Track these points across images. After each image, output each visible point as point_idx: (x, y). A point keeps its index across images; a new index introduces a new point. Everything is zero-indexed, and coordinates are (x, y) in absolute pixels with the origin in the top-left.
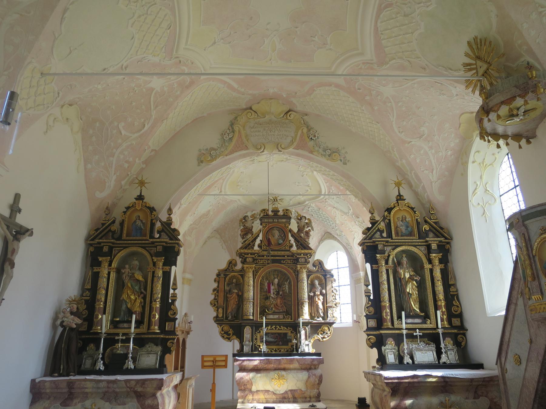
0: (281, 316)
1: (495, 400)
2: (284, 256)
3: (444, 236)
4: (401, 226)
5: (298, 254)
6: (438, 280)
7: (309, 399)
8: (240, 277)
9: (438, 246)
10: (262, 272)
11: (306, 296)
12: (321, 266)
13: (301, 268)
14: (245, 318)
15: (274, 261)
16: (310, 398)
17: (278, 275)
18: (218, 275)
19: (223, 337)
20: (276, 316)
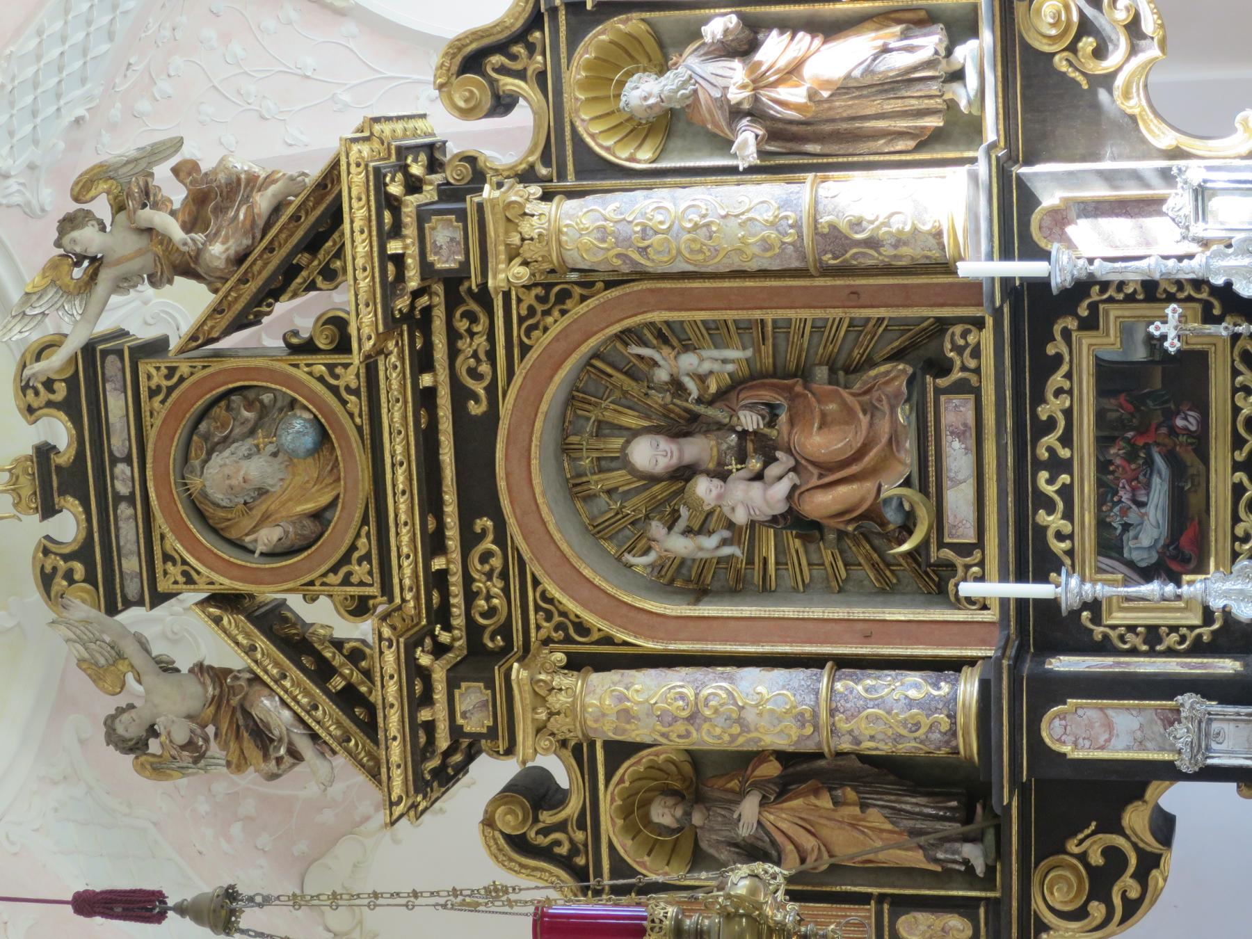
0: (956, 411)
2: (427, 398)
5: (391, 288)
8: (627, 769)
10: (582, 578)
12: (502, 47)
14: (969, 745)
15: (480, 495)
17: (603, 429)
19: (1132, 908)
20: (957, 458)
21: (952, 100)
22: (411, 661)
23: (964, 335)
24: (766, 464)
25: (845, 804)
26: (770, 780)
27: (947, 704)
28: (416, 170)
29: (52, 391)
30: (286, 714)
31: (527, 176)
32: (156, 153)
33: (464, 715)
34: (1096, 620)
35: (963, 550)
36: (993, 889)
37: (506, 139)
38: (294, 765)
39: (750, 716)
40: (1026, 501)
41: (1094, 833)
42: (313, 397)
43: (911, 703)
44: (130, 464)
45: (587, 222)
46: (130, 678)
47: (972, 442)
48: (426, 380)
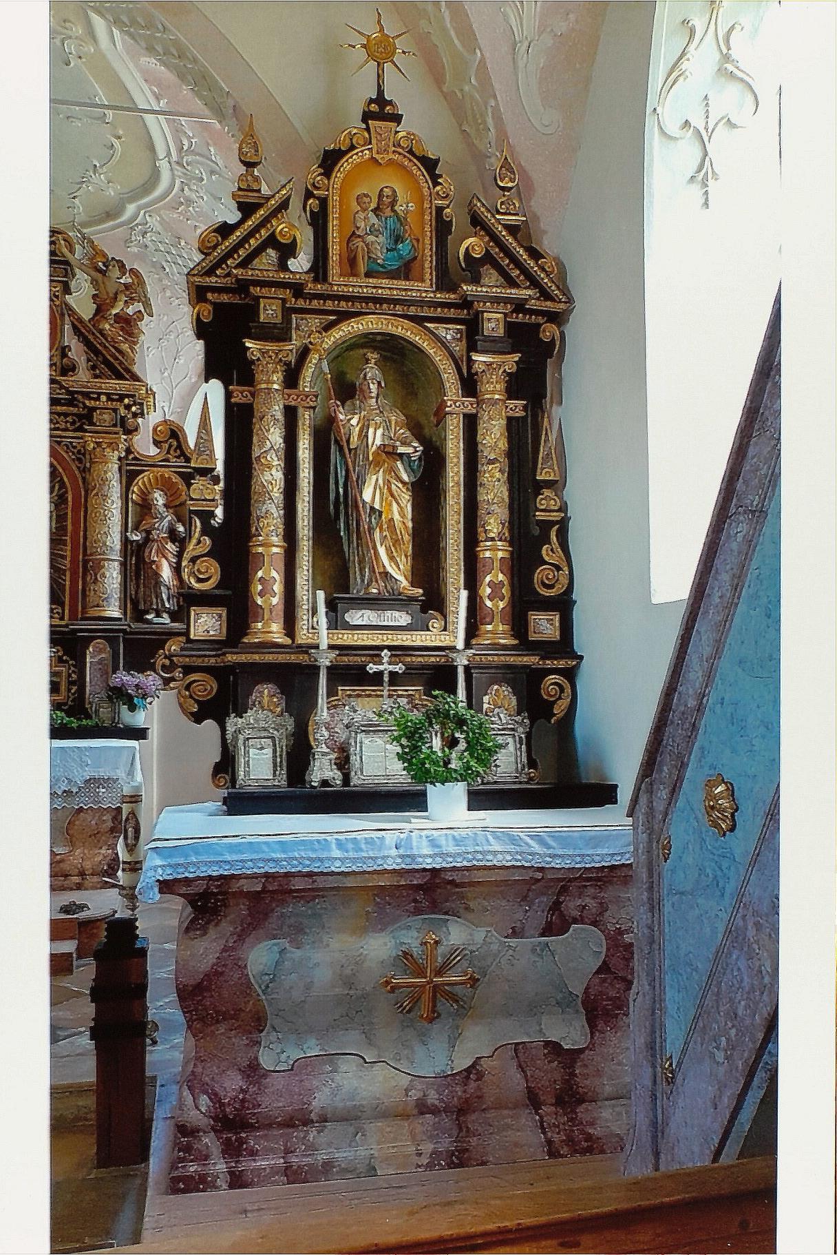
1: (627, 938)
3: (534, 283)
4: (373, 231)
5: (87, 395)
6: (491, 462)
7: (76, 879)
9: (510, 327)
11: (114, 540)
12: (179, 447)
16: (82, 874)
28: (134, 409)
31: (129, 451)
32: (147, 305)
37: (145, 445)
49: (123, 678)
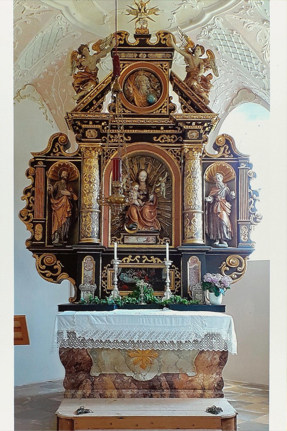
0: (152, 240)
2: (158, 128)
5: (185, 123)
7: (200, 392)
11: (199, 202)
12: (230, 148)
13: (190, 149)
15: (136, 138)
16: (203, 389)
18: (33, 164)
19: (44, 275)
20: (142, 239)
21: (50, 273)
22: (103, 121)
23: (168, 242)
24: (142, 200)
25: (68, 214)
26: (73, 198)
27: (93, 236)
29: (163, 40)
30: (90, 90)
32: (215, 70)
33: (90, 131)
34: (108, 267)
35: (123, 240)
36: (48, 245)
38: (76, 90)
39: (91, 194)
40: (134, 253)
41: (61, 266)
42: (160, 103)
43: (93, 229)
44: (139, 53)
45: (196, 165)
46: (96, 52)
47: (145, 243)
48: (162, 128)
49: (209, 277)
